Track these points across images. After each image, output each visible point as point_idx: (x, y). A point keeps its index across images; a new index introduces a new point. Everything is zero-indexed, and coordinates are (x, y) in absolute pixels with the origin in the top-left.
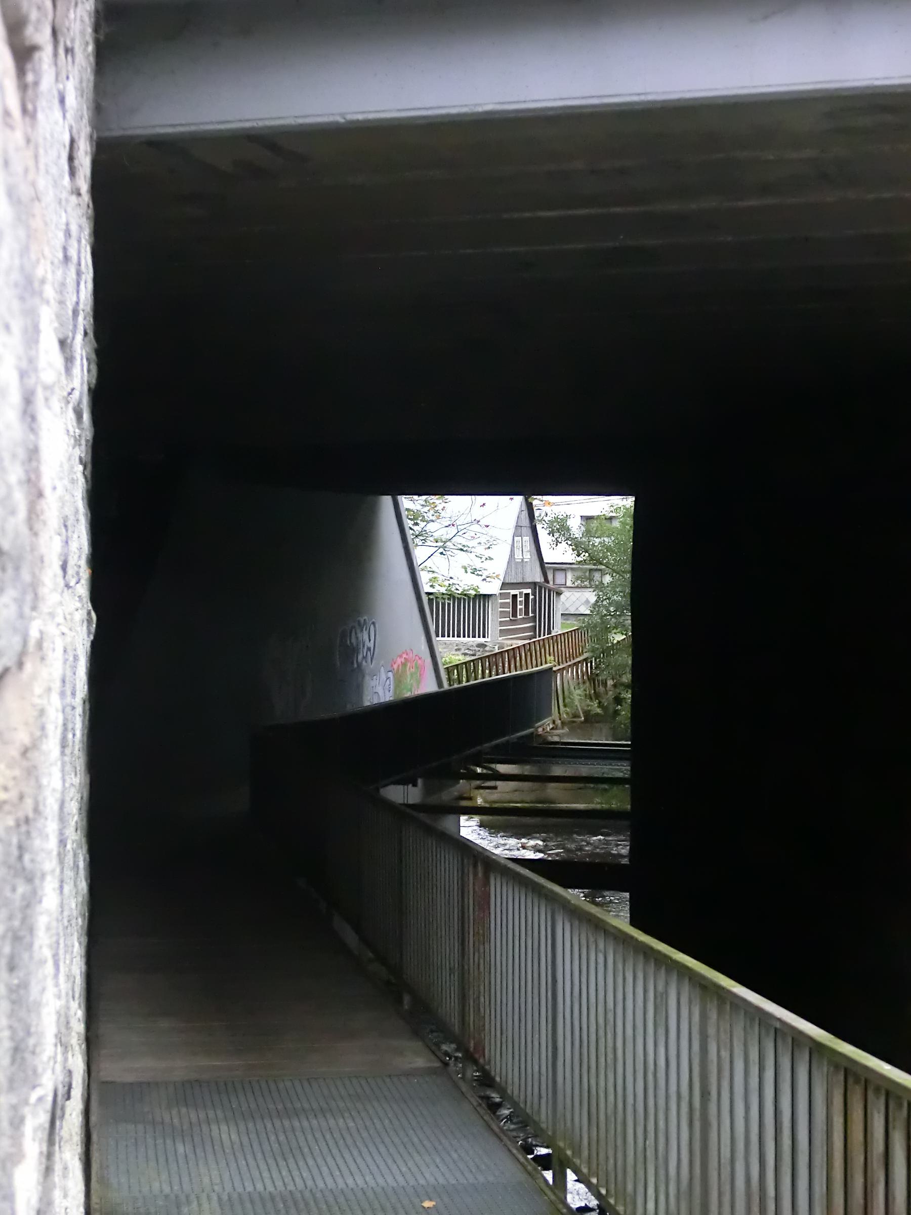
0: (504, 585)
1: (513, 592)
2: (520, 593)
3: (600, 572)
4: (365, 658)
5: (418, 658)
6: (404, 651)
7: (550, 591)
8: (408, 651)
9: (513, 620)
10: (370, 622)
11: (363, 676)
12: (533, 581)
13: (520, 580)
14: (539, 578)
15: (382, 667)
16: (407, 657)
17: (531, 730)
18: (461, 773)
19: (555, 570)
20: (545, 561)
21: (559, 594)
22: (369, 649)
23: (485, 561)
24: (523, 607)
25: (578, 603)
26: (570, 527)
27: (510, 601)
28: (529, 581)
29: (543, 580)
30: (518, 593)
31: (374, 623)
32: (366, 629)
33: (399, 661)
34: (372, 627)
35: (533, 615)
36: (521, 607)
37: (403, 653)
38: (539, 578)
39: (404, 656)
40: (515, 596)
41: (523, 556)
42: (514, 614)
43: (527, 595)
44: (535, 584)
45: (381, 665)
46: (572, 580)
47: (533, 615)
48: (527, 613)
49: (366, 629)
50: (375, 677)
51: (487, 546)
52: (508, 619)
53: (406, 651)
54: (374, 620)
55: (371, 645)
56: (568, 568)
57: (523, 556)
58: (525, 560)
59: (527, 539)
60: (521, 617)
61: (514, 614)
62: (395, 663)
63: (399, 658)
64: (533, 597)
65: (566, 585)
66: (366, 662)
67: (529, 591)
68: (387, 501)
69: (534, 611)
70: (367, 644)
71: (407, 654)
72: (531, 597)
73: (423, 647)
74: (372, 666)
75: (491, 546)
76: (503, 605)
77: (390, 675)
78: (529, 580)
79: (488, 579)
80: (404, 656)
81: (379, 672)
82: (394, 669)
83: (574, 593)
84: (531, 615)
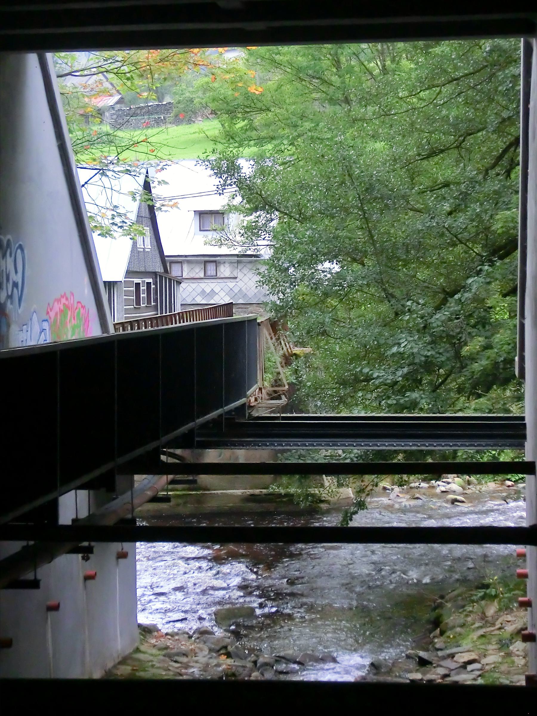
0: (129, 273)
1: (136, 281)
2: (142, 281)
3: (215, 264)
4: (10, 297)
5: (80, 307)
6: (63, 294)
7: (170, 280)
8: (68, 295)
9: (137, 308)
10: (17, 245)
11: (8, 326)
12: (154, 271)
13: (142, 269)
14: (159, 269)
15: (35, 314)
16: (67, 303)
17: (243, 400)
18: (163, 462)
19: (171, 262)
20: (166, 254)
21: (179, 283)
22: (15, 285)
23: (157, 186)
24: (145, 295)
25: (194, 294)
26: (241, 166)
27: (134, 289)
28: (150, 270)
29: (163, 271)
30: (141, 282)
31: (21, 247)
32: (11, 255)
33: (57, 307)
34: (19, 251)
35: (155, 304)
36: (143, 295)
37: (62, 297)
38: (159, 269)
39: (63, 301)
40: (138, 285)
41: (144, 246)
42: (138, 302)
43: (149, 284)
44: (155, 274)
45: (32, 310)
46: (241, 231)
47: (155, 304)
48: (149, 302)
49: (11, 255)
50: (25, 327)
51: (159, 168)
52: (133, 307)
53: (65, 294)
54: (21, 243)
55: (18, 278)
56: (184, 261)
57: (144, 246)
58: (147, 250)
59: (148, 230)
60: (144, 305)
61: (138, 302)
62: (51, 310)
63: (56, 304)
64: (154, 286)
65: (182, 276)
66: (12, 303)
67: (150, 280)
68: (32, 59)
69: (156, 300)
70: (14, 277)
71: (67, 299)
72: (153, 286)
73: (86, 291)
74: (20, 311)
75: (165, 167)
76: (127, 293)
77: (46, 325)
78: (151, 270)
79: (164, 208)
80: (63, 301)
81: (31, 319)
82: (50, 318)
83: (191, 284)
84: (153, 304)
